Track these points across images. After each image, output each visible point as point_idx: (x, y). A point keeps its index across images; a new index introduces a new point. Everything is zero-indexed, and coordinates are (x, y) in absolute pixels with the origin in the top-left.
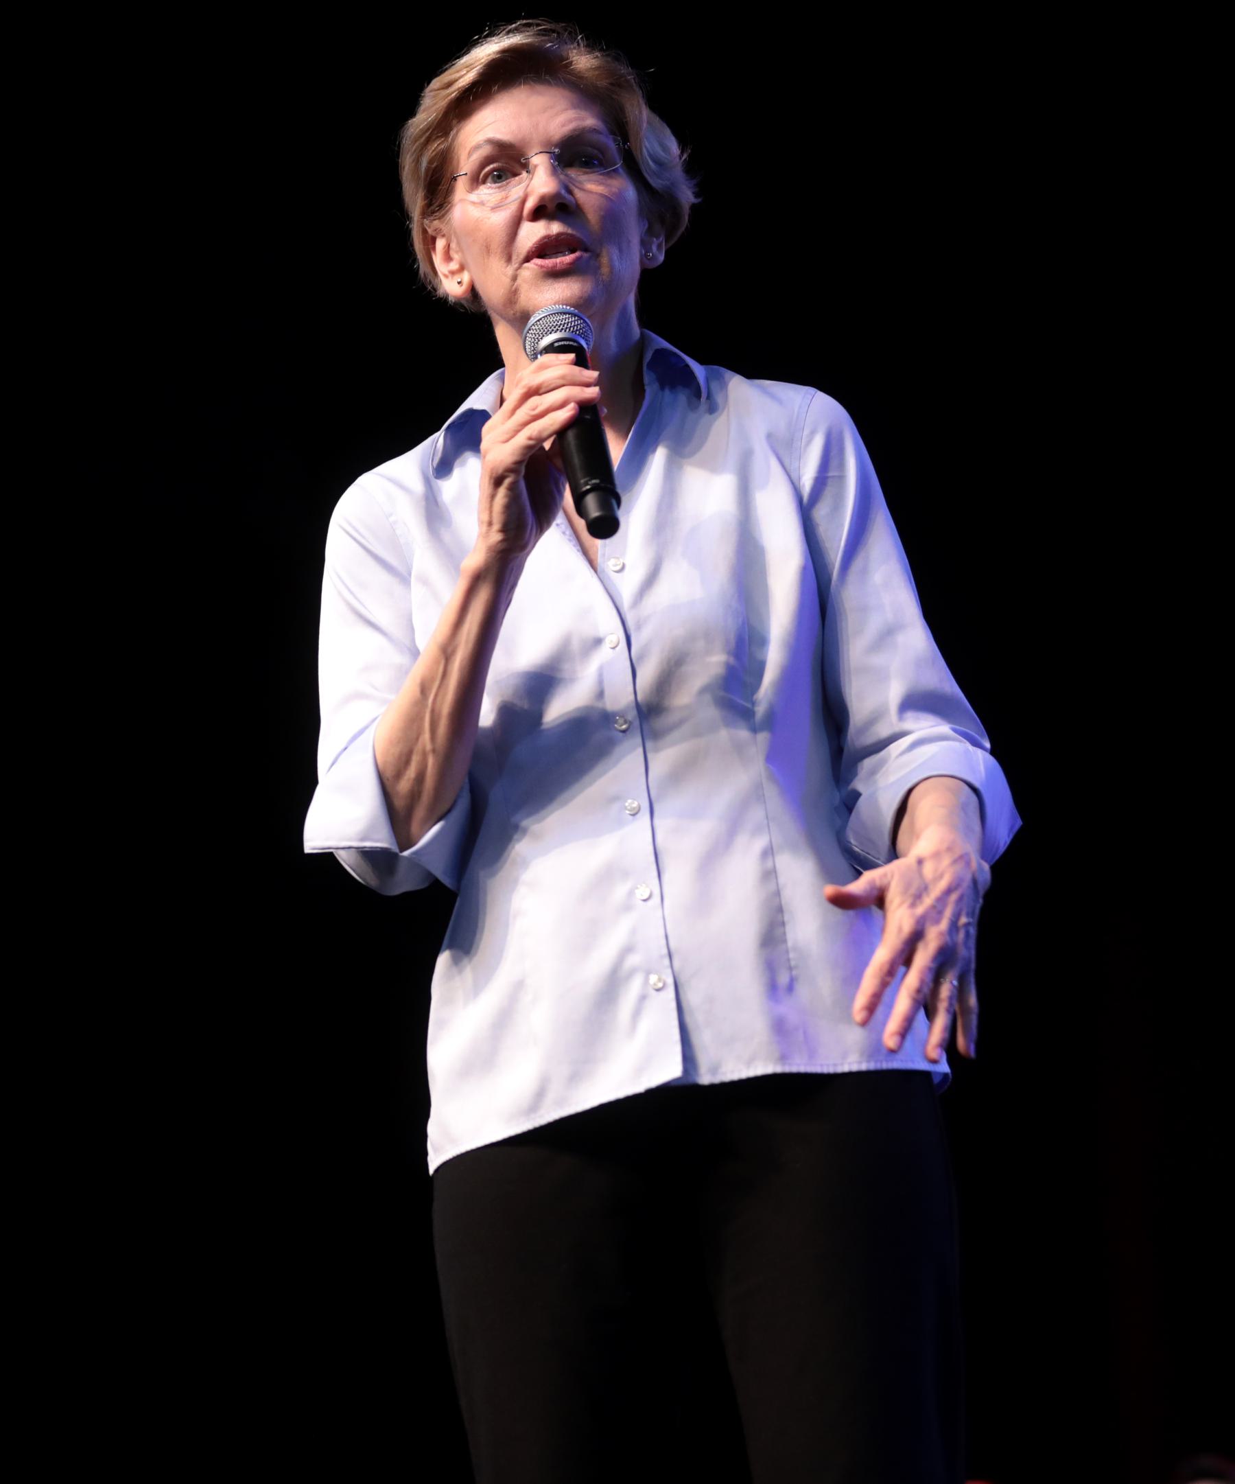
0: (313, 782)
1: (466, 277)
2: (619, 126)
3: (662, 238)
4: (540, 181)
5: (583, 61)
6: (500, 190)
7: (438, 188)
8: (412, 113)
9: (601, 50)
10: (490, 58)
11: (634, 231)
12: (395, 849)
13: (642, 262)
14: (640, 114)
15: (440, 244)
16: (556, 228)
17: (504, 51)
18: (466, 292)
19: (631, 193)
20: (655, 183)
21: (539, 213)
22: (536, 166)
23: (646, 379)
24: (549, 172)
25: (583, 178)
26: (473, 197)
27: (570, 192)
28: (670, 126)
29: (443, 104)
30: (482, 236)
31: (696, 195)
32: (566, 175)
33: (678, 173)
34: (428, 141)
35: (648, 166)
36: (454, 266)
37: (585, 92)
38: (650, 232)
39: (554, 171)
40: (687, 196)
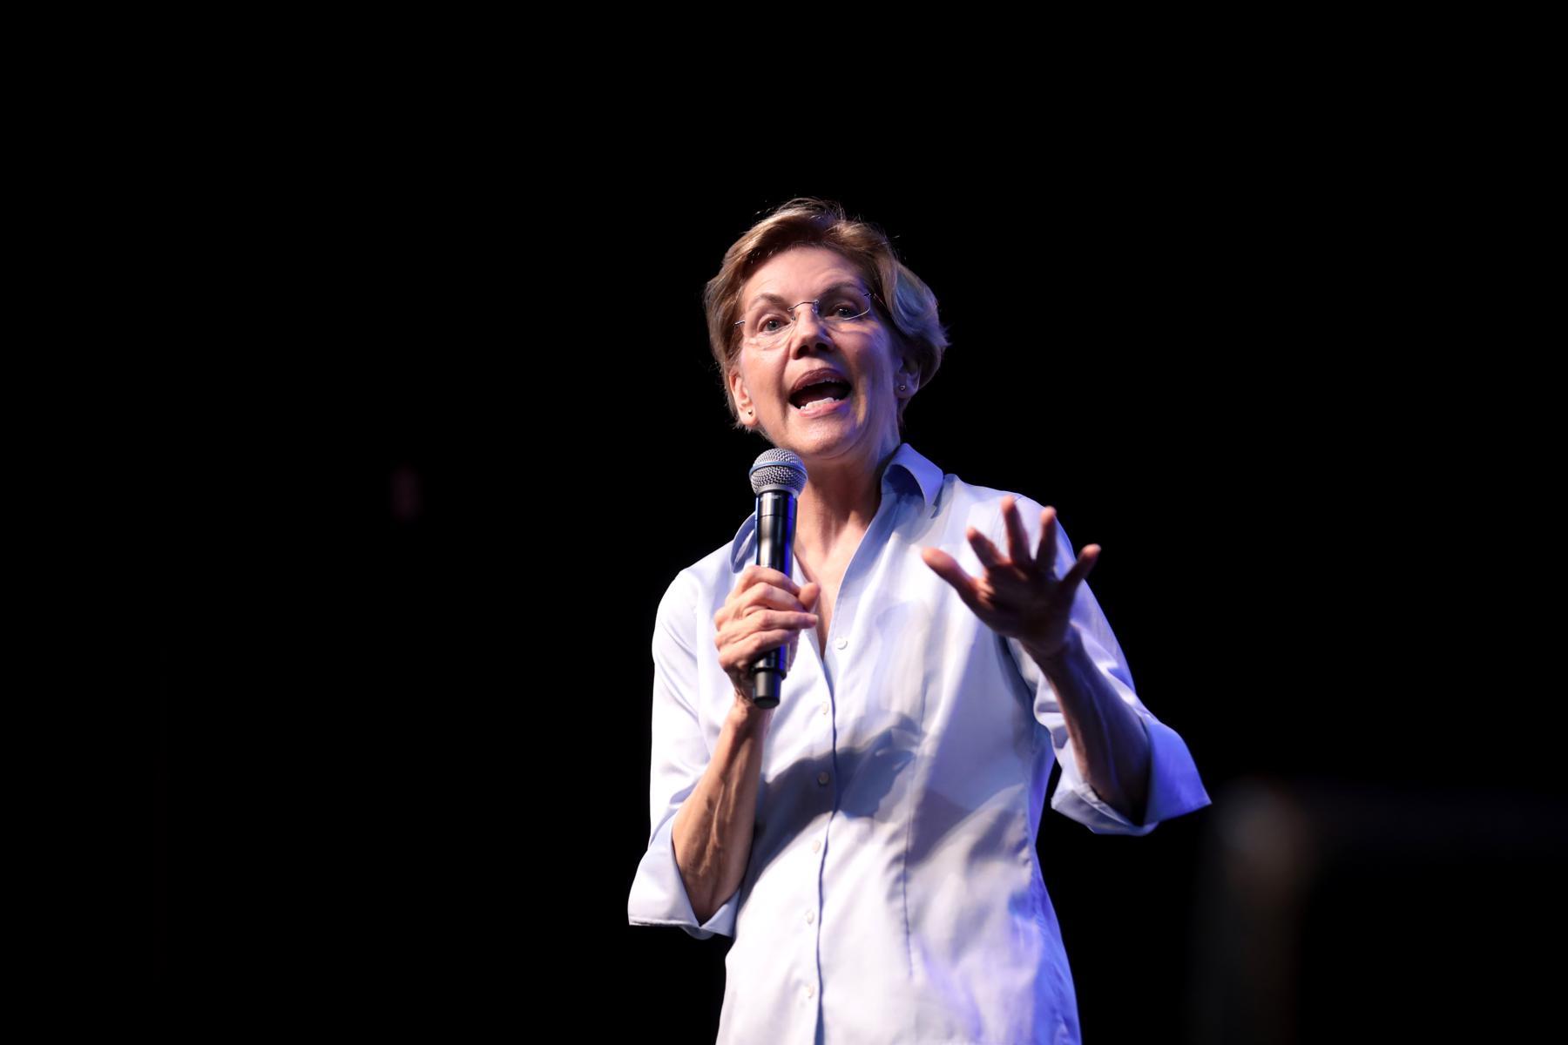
2: (874, 286)
3: (917, 374)
4: (802, 327)
5: (847, 230)
6: (783, 316)
7: (732, 336)
9: (863, 221)
12: (696, 924)
14: (892, 270)
15: (739, 381)
16: (817, 364)
20: (909, 331)
21: (802, 352)
23: (884, 489)
25: (938, 349)
26: (753, 341)
27: (828, 335)
31: (948, 340)
32: (1021, 845)
34: (723, 298)
36: (746, 401)
39: (814, 319)
40: (940, 341)
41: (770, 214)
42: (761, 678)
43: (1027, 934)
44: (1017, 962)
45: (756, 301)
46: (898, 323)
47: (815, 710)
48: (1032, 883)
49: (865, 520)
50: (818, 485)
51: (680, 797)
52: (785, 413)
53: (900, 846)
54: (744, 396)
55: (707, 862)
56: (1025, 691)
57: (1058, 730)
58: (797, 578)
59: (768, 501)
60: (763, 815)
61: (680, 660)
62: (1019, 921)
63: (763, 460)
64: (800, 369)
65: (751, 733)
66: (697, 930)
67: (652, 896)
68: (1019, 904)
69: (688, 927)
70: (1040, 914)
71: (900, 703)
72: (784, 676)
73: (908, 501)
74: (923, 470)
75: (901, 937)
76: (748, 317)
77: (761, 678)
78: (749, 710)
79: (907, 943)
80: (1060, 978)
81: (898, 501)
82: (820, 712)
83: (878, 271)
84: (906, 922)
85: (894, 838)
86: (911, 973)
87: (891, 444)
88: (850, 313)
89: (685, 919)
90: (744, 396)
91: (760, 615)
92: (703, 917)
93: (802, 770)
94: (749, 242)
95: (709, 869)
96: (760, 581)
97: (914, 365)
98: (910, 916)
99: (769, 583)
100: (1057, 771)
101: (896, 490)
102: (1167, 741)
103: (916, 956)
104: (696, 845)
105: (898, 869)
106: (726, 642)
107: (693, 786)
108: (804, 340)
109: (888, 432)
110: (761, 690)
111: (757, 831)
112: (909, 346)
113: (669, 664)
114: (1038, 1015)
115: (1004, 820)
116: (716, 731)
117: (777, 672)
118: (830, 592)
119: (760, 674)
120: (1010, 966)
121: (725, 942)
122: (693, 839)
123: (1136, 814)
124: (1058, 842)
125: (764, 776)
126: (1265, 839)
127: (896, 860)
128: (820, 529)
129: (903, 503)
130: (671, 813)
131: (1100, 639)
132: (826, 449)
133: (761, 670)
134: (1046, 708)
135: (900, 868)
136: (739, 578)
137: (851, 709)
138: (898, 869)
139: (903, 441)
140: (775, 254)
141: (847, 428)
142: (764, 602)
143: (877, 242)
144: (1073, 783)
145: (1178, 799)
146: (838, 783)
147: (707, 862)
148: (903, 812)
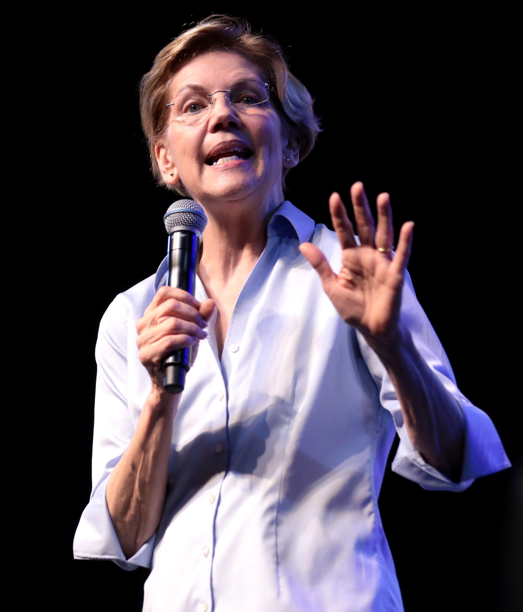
1: (175, 171)
4: (218, 109)
5: (250, 41)
6: (197, 113)
8: (148, 69)
10: (191, 36)
11: (279, 145)
12: (123, 558)
13: (283, 165)
15: (162, 152)
16: (229, 137)
17: (200, 32)
18: (176, 180)
20: (294, 118)
21: (217, 128)
22: (216, 99)
24: (223, 103)
26: (179, 118)
27: (237, 116)
28: (306, 87)
29: (164, 63)
31: (321, 127)
32: (366, 502)
34: (156, 87)
35: (289, 109)
36: (169, 165)
37: (250, 57)
38: (290, 146)
39: (227, 104)
40: (315, 127)
41: (194, 26)
42: (170, 370)
43: (368, 568)
44: (359, 589)
45: (182, 90)
46: (287, 111)
47: (214, 397)
48: (374, 530)
49: (256, 252)
50: (223, 223)
51: (112, 464)
52: (201, 170)
53: (274, 498)
55: (131, 511)
57: (397, 413)
60: (175, 476)
61: (115, 360)
62: (362, 557)
64: (214, 140)
65: (163, 414)
66: (124, 563)
67: (91, 538)
68: (363, 546)
69: (118, 560)
70: (379, 554)
71: (278, 388)
72: (187, 370)
73: (288, 244)
74: (298, 219)
75: (273, 566)
76: (175, 101)
77: (170, 370)
78: (162, 396)
79: (277, 571)
80: (392, 602)
81: (280, 243)
82: (217, 399)
83: (273, 71)
84: (277, 555)
85: (271, 491)
86: (279, 594)
87: (277, 202)
88: (250, 101)
89: (115, 554)
91: (171, 322)
93: (203, 440)
94: (177, 46)
97: (295, 144)
98: (279, 551)
100: (397, 441)
101: (278, 235)
102: (479, 420)
103: (283, 581)
104: (123, 499)
106: (145, 342)
107: (121, 456)
108: (220, 119)
109: (276, 191)
111: (169, 489)
112: (294, 130)
113: (107, 363)
116: (138, 412)
117: (182, 367)
118: (227, 308)
119: (170, 367)
121: (144, 573)
122: (122, 494)
123: (454, 472)
124: (396, 498)
125: (175, 446)
127: (271, 509)
128: (222, 263)
129: (284, 245)
130: (106, 475)
132: (232, 194)
133: (170, 364)
134: (389, 397)
135: (272, 515)
137: (239, 396)
139: (286, 199)
140: (197, 55)
141: (249, 178)
143: (273, 50)
144: (407, 451)
146: (231, 450)
147: (131, 511)
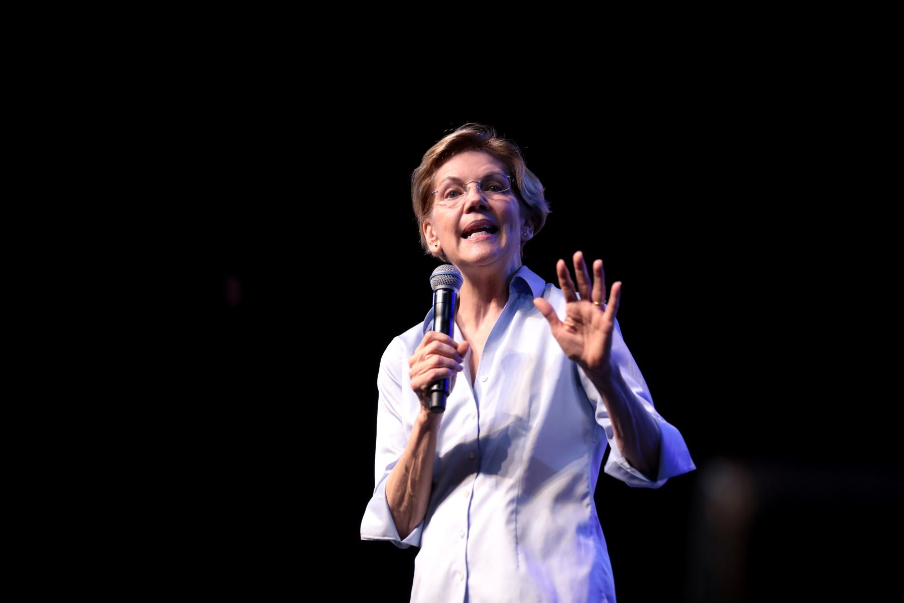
0: (371, 496)
1: (439, 243)
2: (510, 171)
4: (471, 196)
5: (496, 143)
6: (456, 198)
7: (427, 200)
8: (418, 165)
11: (518, 223)
12: (399, 539)
14: (521, 168)
15: (429, 228)
16: (480, 217)
17: (457, 136)
19: (515, 207)
20: (530, 202)
21: (471, 210)
23: (511, 291)
26: (442, 203)
29: (430, 160)
30: (445, 224)
31: (550, 209)
32: (585, 496)
33: (542, 197)
34: (424, 179)
35: (526, 195)
36: (434, 238)
38: (526, 224)
39: (478, 191)
40: (545, 209)
42: (435, 396)
43: (587, 546)
45: (444, 181)
46: (525, 198)
47: (468, 416)
48: (591, 518)
49: (501, 305)
52: (458, 242)
53: (514, 493)
54: (432, 236)
55: (405, 503)
56: (589, 406)
57: (609, 428)
58: (457, 338)
59: (440, 295)
60: (438, 476)
61: (393, 388)
62: (582, 539)
63: (438, 271)
64: (468, 219)
65: (429, 428)
66: (399, 543)
67: (374, 523)
68: (582, 530)
69: (395, 541)
70: (595, 536)
71: (517, 409)
72: (448, 395)
73: (525, 299)
75: (513, 545)
76: (438, 189)
77: (435, 396)
78: (429, 415)
79: (516, 549)
80: (605, 572)
81: (519, 297)
82: (470, 418)
83: (514, 167)
84: (516, 537)
85: (512, 487)
86: (518, 567)
88: (496, 189)
89: (392, 537)
90: (432, 236)
91: (435, 358)
92: (403, 535)
93: (460, 449)
94: (440, 147)
95: (407, 507)
96: (435, 340)
97: (530, 222)
98: (518, 534)
99: (440, 341)
100: (608, 449)
102: (671, 433)
104: (399, 494)
105: (513, 507)
106: (416, 374)
108: (473, 203)
109: (516, 258)
110: (434, 403)
111: (434, 486)
112: (529, 211)
114: (591, 593)
115: (575, 480)
116: (410, 428)
117: (444, 393)
118: (478, 347)
119: (434, 393)
120: (577, 562)
121: (414, 550)
124: (607, 493)
125: (438, 454)
126: (728, 492)
127: (512, 501)
129: (522, 299)
130: (386, 476)
131: (633, 375)
134: (602, 416)
136: (424, 340)
137: (488, 415)
138: (513, 507)
140: (455, 154)
142: (435, 352)
144: (616, 457)
145: (677, 466)
146: (482, 457)
147: (405, 503)
148: (517, 471)
